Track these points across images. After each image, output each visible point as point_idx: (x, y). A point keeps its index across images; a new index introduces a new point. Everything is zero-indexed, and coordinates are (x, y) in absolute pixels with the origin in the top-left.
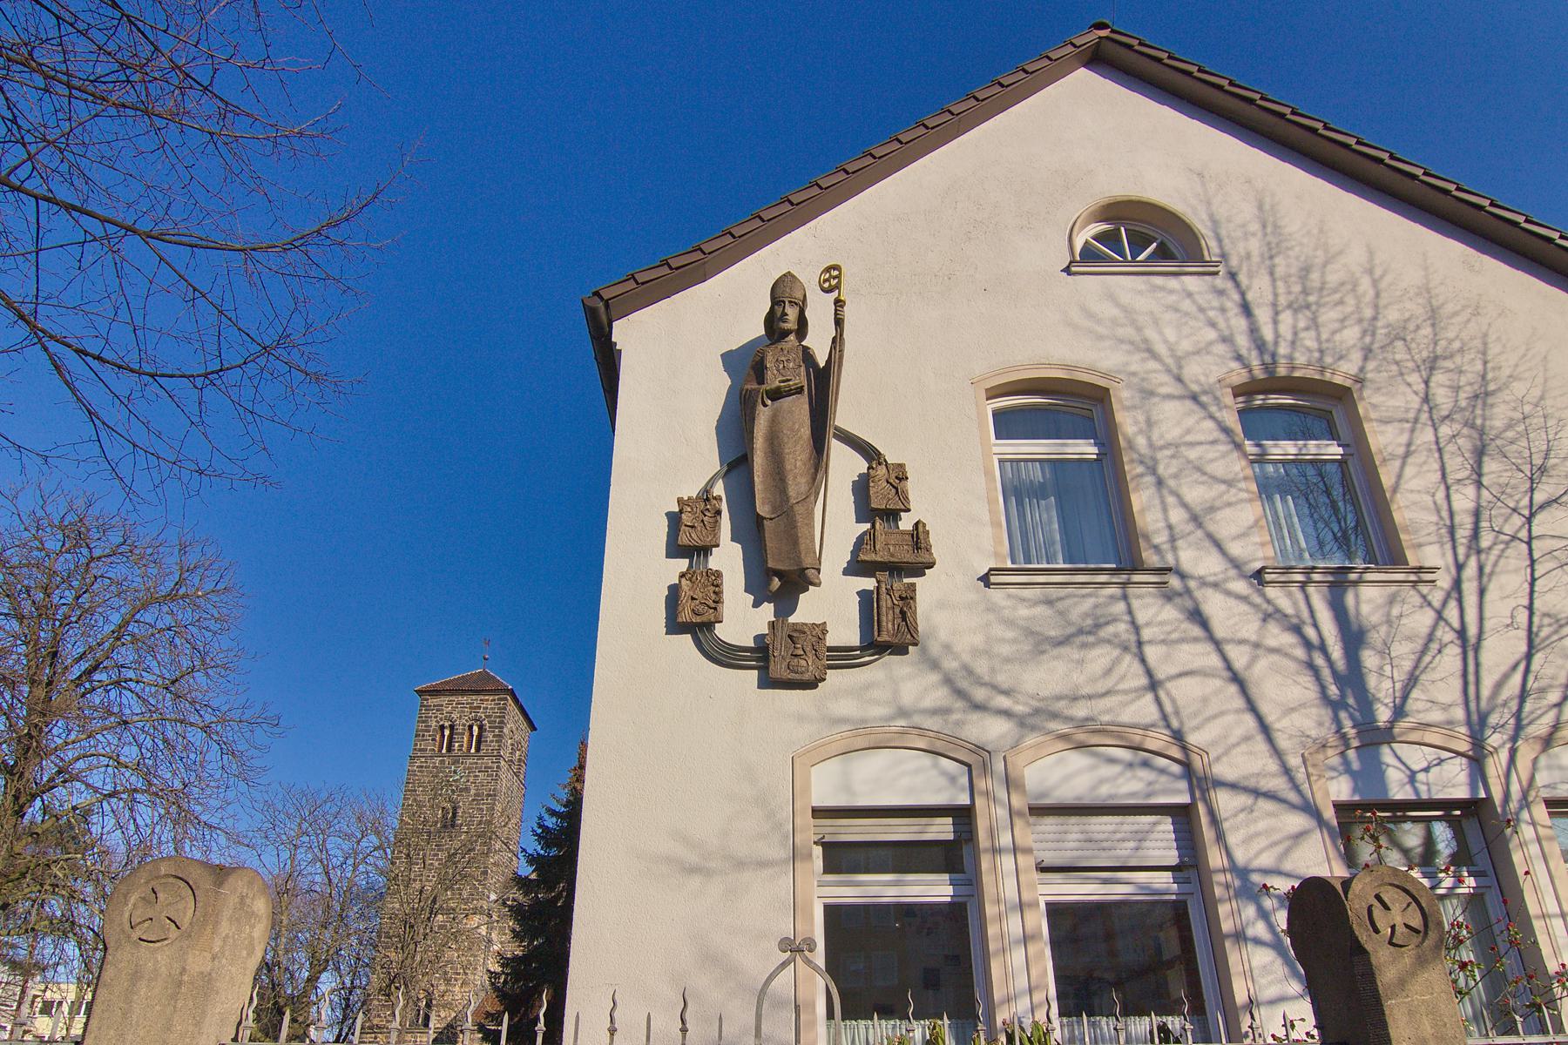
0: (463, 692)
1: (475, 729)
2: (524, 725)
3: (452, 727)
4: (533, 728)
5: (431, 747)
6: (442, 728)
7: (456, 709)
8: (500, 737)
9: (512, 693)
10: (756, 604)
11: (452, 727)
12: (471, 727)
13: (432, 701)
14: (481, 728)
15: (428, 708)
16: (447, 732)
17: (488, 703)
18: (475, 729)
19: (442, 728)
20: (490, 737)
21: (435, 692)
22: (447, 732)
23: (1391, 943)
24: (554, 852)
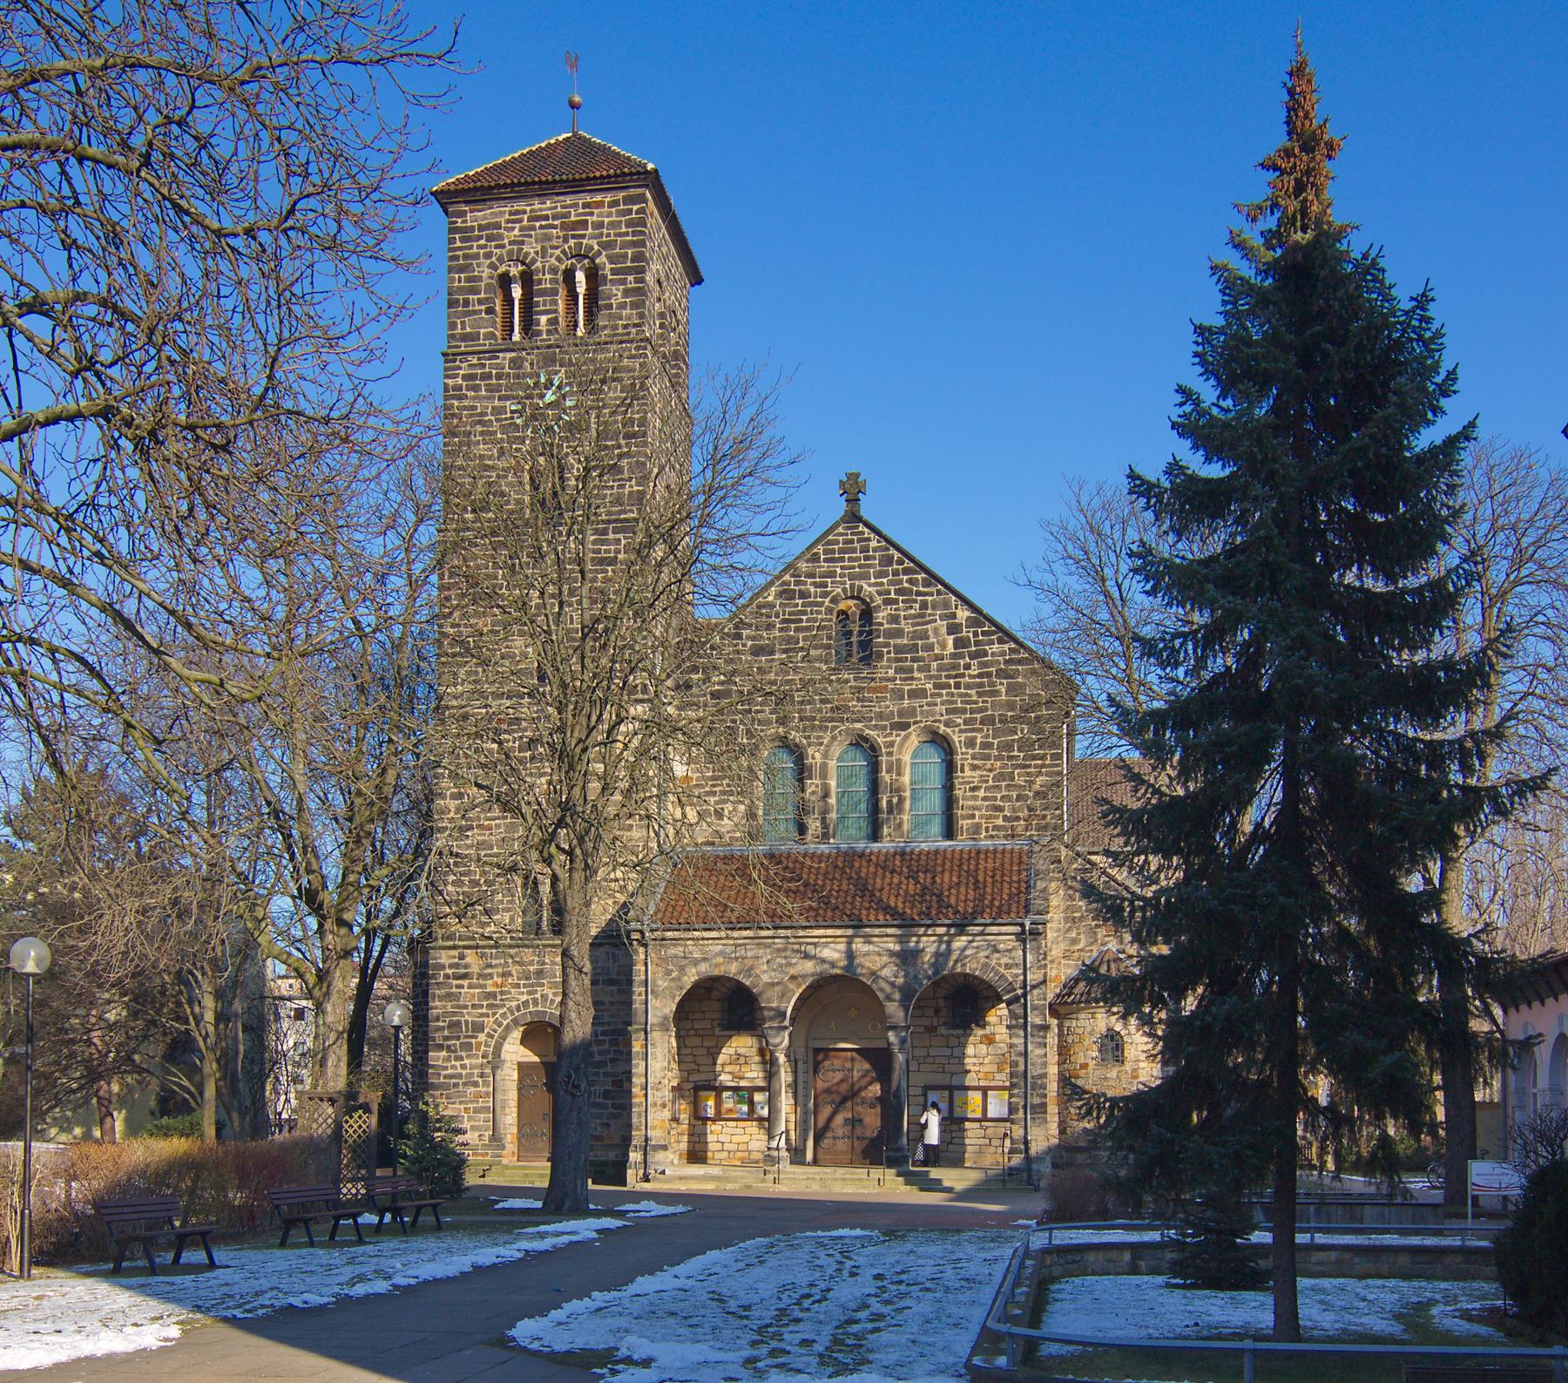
0: (544, 189)
1: (580, 277)
2: (678, 270)
3: (527, 279)
4: (696, 279)
5: (487, 329)
6: (505, 281)
7: (526, 232)
8: (638, 294)
9: (653, 180)
10: (1433, 300)
11: (527, 279)
12: (569, 276)
13: (475, 217)
14: (593, 276)
15: (467, 234)
16: (517, 292)
17: (603, 212)
18: (580, 277)
19: (505, 281)
20: (615, 294)
21: (477, 192)
22: (517, 292)
23: (74, 74)
24: (1215, 471)
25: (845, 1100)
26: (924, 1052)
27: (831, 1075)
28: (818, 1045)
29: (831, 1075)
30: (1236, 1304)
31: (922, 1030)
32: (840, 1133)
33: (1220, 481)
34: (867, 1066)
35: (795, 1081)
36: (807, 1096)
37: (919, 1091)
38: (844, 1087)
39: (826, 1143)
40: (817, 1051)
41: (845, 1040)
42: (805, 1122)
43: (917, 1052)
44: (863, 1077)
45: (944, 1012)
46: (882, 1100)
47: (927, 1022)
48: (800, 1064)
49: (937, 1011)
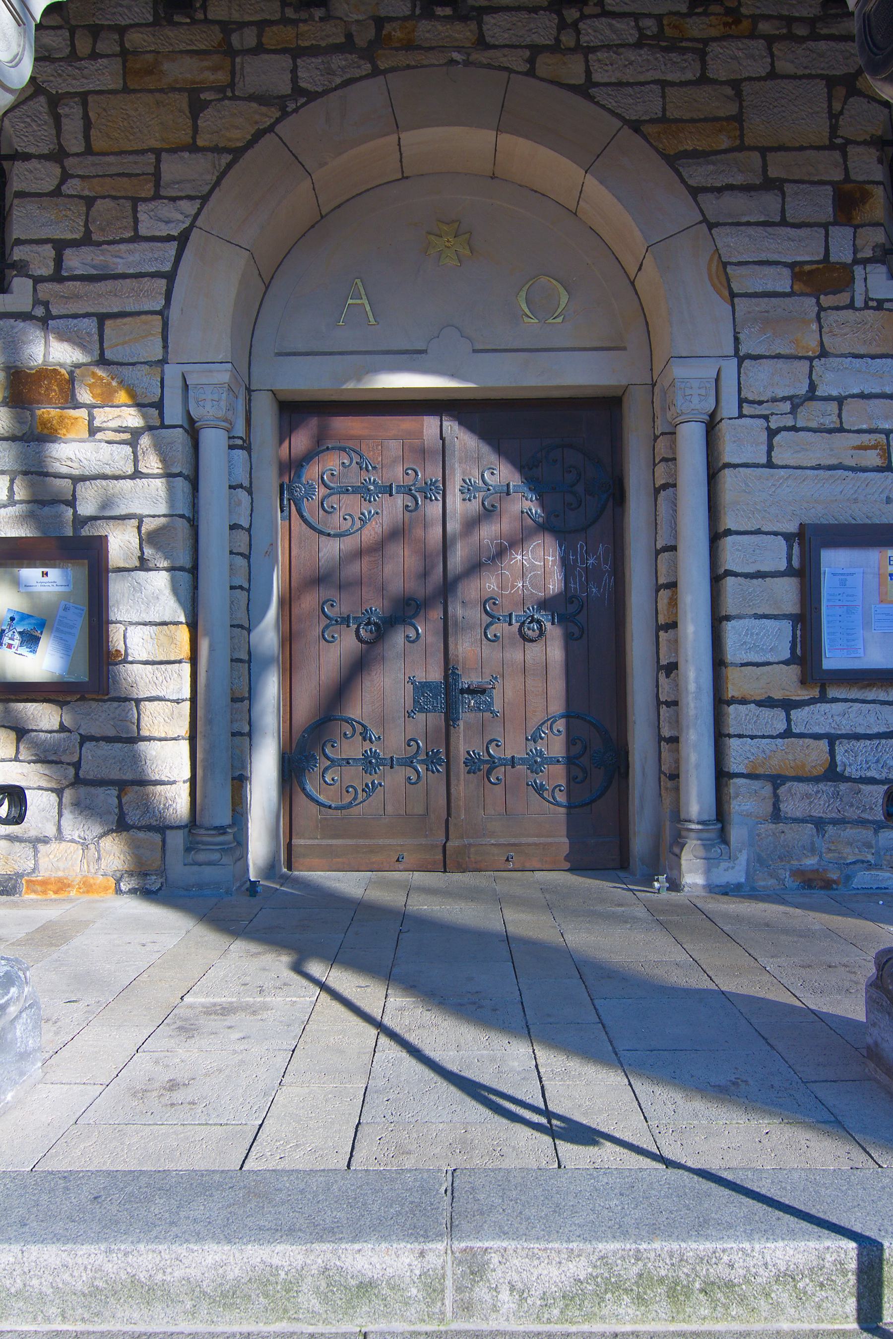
25: (405, 610)
26: (789, 380)
27: (351, 512)
28: (307, 379)
29: (351, 512)
30: (741, 905)
31: (782, 281)
32: (393, 743)
33: (569, 639)
34: (503, 474)
35: (190, 518)
36: (247, 592)
37: (774, 555)
38: (399, 569)
39: (324, 784)
40: (293, 411)
41: (411, 358)
42: (243, 699)
43: (764, 380)
44: (488, 512)
45: (877, 206)
46: (565, 608)
47: (806, 249)
48: (213, 441)
49: (847, 202)
